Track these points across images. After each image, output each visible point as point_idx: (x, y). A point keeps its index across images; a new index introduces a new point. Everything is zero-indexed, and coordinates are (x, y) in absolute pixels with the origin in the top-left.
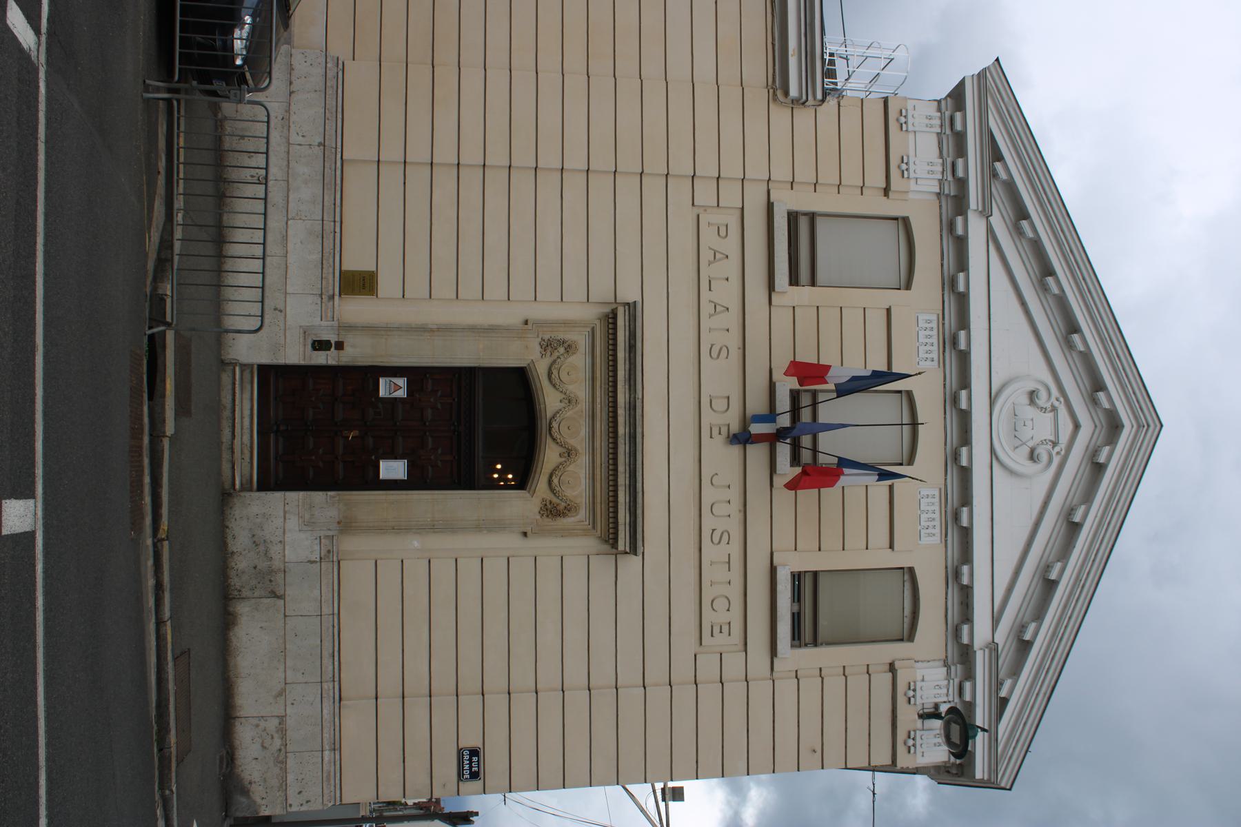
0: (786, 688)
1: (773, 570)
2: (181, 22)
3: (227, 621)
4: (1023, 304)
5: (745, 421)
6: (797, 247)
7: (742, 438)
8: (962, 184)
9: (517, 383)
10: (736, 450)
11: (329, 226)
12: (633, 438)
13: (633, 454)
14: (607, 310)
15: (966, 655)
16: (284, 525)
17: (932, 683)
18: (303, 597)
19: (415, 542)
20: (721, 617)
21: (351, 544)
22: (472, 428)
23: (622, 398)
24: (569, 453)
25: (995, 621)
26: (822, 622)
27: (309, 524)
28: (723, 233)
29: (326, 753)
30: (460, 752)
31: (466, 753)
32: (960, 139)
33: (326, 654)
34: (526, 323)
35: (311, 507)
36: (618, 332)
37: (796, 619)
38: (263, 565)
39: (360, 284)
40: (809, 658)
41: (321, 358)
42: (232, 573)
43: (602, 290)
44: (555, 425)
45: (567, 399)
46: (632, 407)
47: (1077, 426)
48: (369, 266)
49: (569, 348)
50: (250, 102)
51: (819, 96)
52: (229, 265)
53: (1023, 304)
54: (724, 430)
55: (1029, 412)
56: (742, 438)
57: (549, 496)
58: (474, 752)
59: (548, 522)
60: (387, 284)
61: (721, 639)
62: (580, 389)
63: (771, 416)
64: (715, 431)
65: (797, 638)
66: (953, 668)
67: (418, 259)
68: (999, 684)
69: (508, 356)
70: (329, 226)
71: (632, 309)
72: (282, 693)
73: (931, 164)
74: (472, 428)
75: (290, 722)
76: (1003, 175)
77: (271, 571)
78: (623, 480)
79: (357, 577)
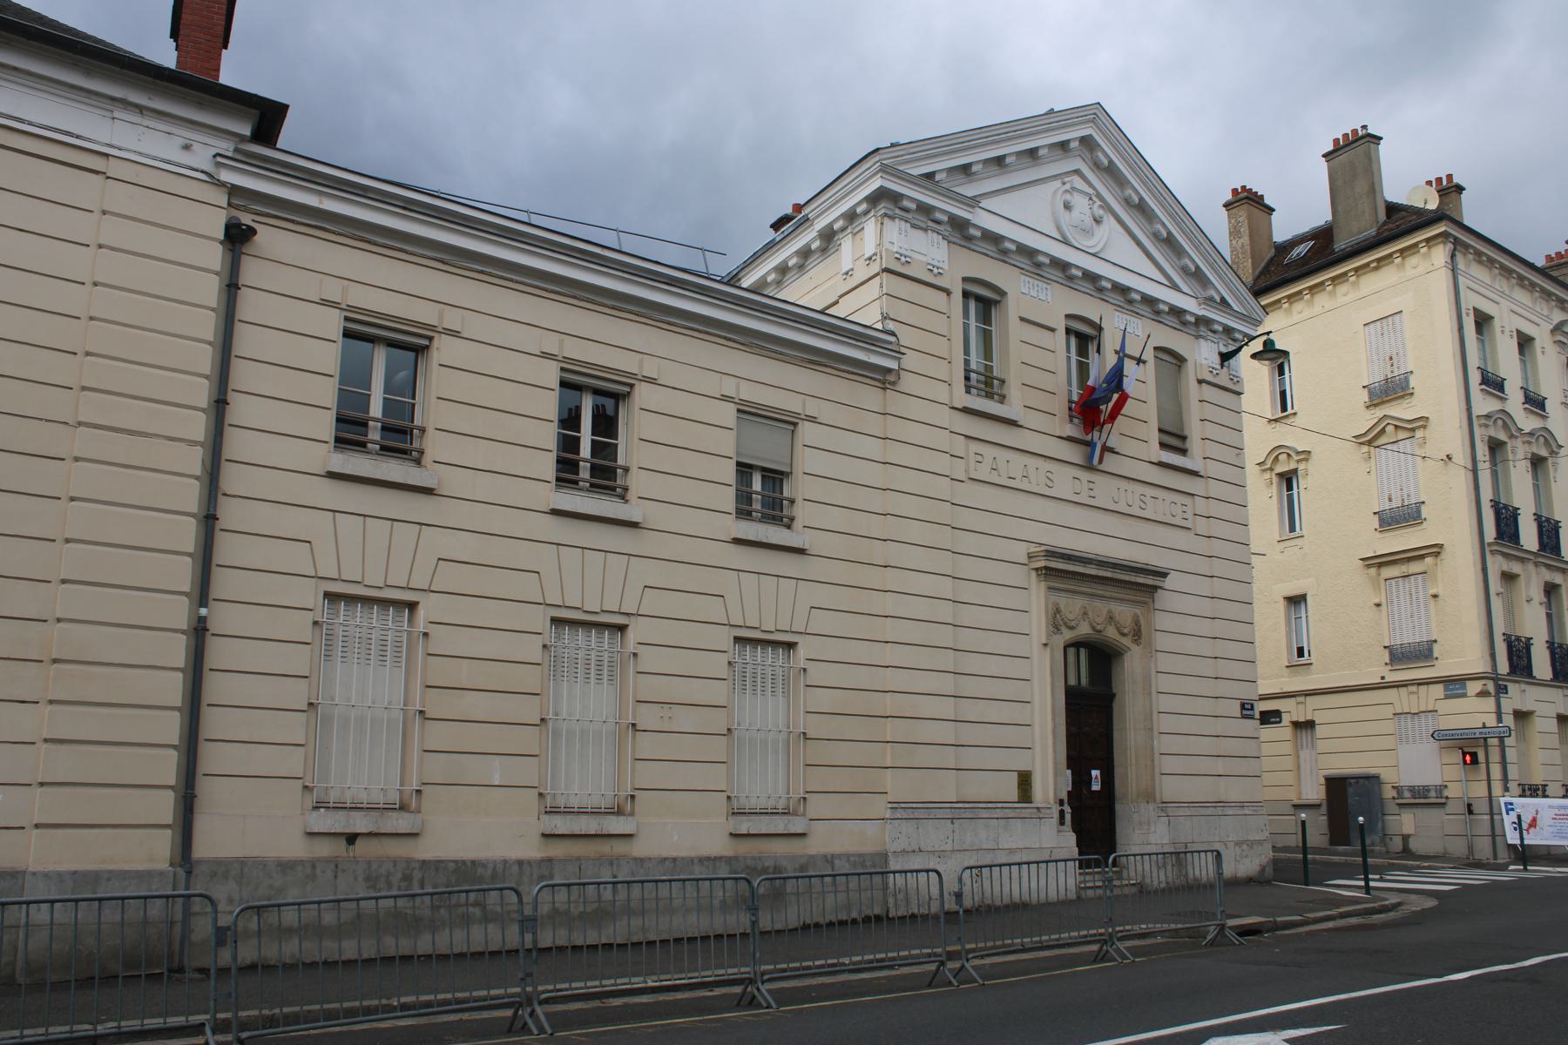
11: (999, 813)
14: (1034, 574)
15: (1201, 321)
16: (1144, 835)
18: (1194, 832)
20: (1178, 510)
24: (1111, 618)
25: (1175, 287)
39: (1025, 780)
41: (1068, 817)
43: (1018, 576)
47: (1077, 172)
50: (535, 908)
51: (892, 339)
52: (998, 903)
55: (1075, 213)
58: (1243, 706)
70: (999, 813)
71: (1051, 554)
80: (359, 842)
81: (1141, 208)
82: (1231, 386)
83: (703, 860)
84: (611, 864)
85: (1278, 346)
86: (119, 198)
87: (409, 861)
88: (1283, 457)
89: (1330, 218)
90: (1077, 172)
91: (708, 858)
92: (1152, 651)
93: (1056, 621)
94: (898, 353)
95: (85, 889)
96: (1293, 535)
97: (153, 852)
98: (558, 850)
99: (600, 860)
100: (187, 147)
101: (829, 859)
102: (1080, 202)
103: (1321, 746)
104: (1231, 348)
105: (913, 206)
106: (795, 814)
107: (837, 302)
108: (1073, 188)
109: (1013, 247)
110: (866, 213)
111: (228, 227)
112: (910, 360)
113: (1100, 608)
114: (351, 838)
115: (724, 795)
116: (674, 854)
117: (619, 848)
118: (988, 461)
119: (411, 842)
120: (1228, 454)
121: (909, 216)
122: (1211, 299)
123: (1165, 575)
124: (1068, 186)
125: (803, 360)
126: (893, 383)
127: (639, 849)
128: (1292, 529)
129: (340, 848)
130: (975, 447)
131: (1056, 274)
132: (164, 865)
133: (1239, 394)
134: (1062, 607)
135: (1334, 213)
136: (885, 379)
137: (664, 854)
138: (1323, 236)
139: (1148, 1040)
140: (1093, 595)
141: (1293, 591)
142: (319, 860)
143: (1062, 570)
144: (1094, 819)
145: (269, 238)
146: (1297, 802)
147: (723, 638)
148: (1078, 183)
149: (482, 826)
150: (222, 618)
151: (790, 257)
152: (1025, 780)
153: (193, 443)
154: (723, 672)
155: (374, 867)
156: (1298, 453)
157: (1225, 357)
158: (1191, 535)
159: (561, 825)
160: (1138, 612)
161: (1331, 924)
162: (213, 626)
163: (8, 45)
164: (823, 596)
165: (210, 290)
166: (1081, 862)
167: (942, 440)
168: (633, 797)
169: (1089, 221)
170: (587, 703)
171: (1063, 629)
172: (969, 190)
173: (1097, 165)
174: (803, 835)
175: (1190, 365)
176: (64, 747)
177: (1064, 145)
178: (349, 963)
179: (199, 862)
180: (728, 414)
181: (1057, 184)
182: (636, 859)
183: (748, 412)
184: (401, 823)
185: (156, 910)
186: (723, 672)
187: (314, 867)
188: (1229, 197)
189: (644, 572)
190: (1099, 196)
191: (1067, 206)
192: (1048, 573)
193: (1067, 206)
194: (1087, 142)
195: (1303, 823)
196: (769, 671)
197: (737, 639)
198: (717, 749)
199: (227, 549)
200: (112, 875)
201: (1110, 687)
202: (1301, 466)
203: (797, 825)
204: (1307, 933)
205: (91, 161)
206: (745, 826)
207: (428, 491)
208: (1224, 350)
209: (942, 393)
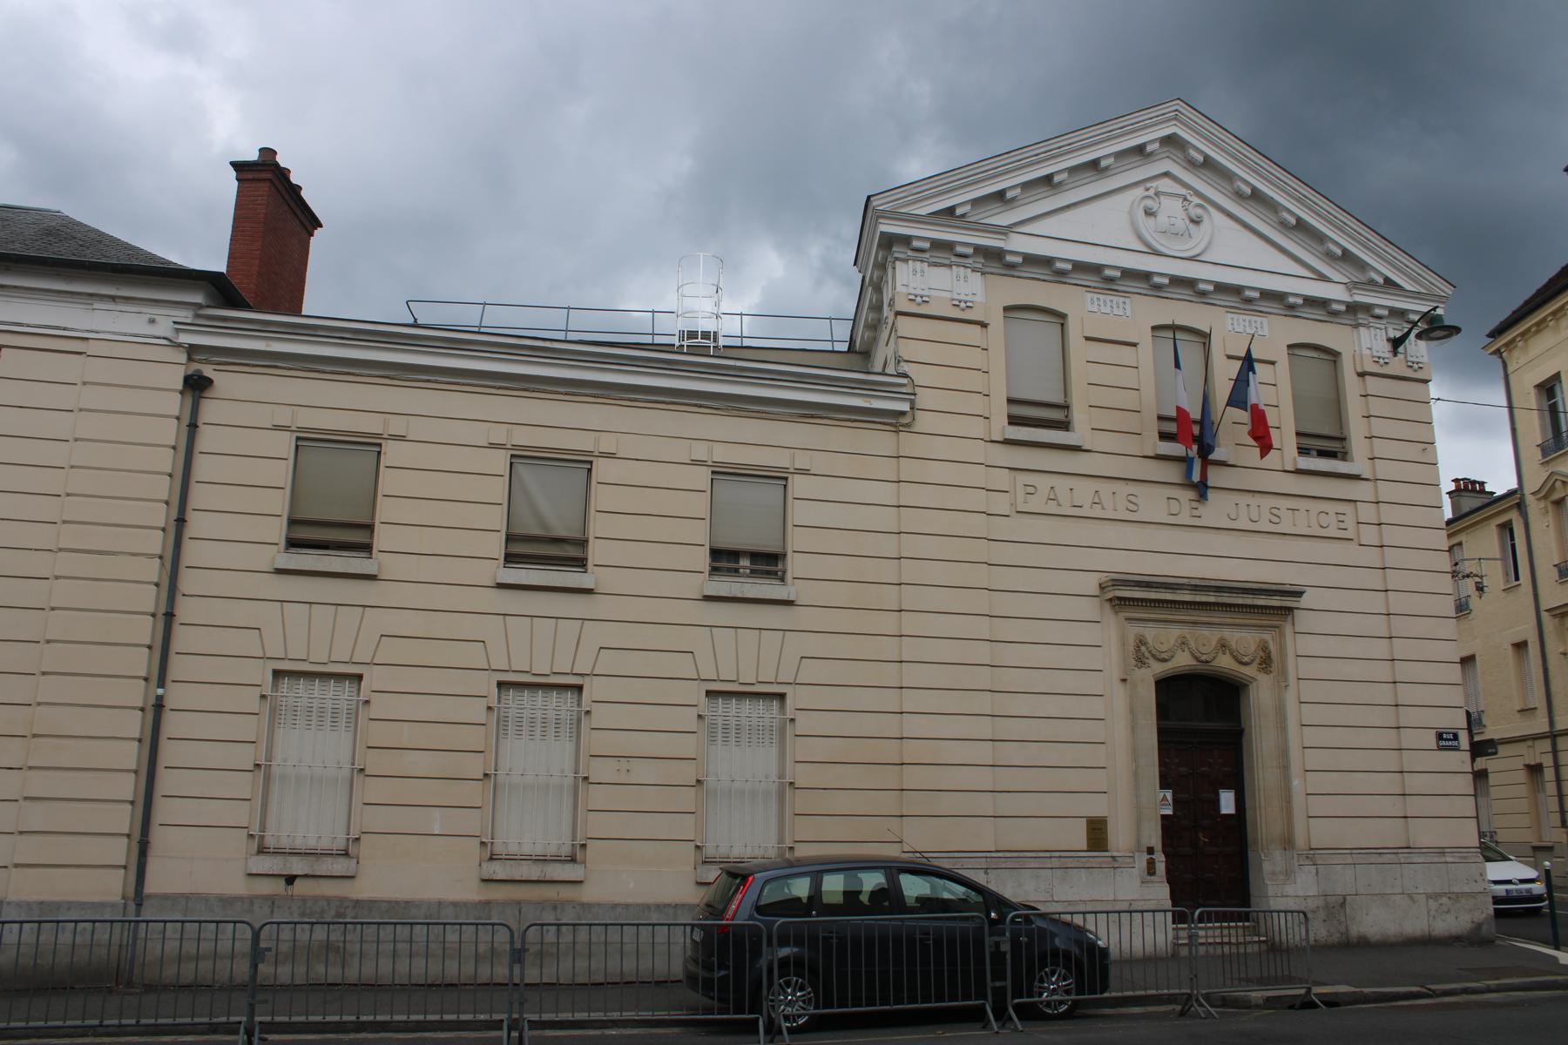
0: (1383, 469)
3: (1364, 944)
4: (1068, 207)
5: (1188, 484)
6: (1039, 418)
7: (1201, 489)
8: (979, 250)
9: (1170, 688)
10: (1211, 494)
11: (1056, 863)
12: (1219, 589)
13: (1231, 590)
14: (1107, 605)
15: (1353, 308)
16: (1286, 889)
17: (1368, 343)
18: (1344, 880)
19: (1296, 783)
20: (1331, 520)
21: (1300, 841)
22: (1202, 726)
23: (1186, 597)
24: (1223, 646)
25: (1323, 278)
26: (1326, 431)
27: (1289, 874)
28: (1031, 490)
29: (1449, 859)
30: (1440, 748)
32: (937, 245)
33: (1380, 860)
34: (1124, 680)
35: (1274, 873)
36: (1131, 597)
37: (1323, 454)
38: (1322, 914)
39: (1097, 832)
40: (1357, 445)
41: (1161, 867)
42: (1330, 940)
43: (1089, 609)
44: (1204, 658)
45: (1184, 646)
47: (1166, 174)
48: (1082, 826)
49: (1141, 642)
51: (904, 381)
53: (1068, 207)
54: (1195, 504)
55: (1162, 218)
56: (1201, 489)
57: (1255, 665)
58: (1440, 736)
59: (1275, 666)
60: (1096, 808)
61: (1350, 523)
62: (1175, 632)
63: (1185, 461)
64: (1196, 513)
65: (1343, 455)
67: (1073, 780)
68: (1372, 282)
69: (1148, 696)
70: (1056, 863)
72: (1410, 896)
73: (915, 272)
74: (1202, 726)
75: (1429, 890)
76: (967, 208)
77: (1326, 907)
78: (1249, 600)
79: (1321, 834)
80: (297, 882)
82: (1409, 373)
83: (660, 907)
84: (555, 908)
86: (97, 370)
87: (342, 900)
90: (1166, 174)
92: (1282, 683)
93: (1141, 654)
95: (46, 916)
97: (110, 888)
98: (499, 893)
99: (541, 905)
100: (152, 321)
101: (372, 904)
111: (187, 379)
114: (290, 880)
116: (630, 901)
117: (566, 893)
119: (347, 882)
120: (1412, 452)
121: (970, 261)
123: (1299, 594)
124: (1151, 192)
125: (791, 415)
127: (589, 894)
129: (279, 887)
132: (117, 898)
133: (1426, 381)
136: (896, 422)
137: (618, 900)
140: (1195, 623)
142: (257, 897)
144: (1209, 856)
145: (224, 381)
147: (695, 693)
148: (1165, 185)
149: (420, 868)
150: (175, 696)
153: (151, 556)
154: (481, 716)
155: (309, 904)
157: (1396, 343)
158: (1353, 546)
159: (499, 870)
162: (170, 703)
163: (8, 270)
164: (814, 645)
165: (169, 432)
166: (1174, 913)
167: (977, 476)
170: (536, 758)
171: (1152, 661)
172: (1003, 219)
173: (1192, 164)
176: (38, 803)
178: (285, 988)
179: (149, 896)
181: (1139, 192)
182: (582, 905)
184: (339, 866)
185: (102, 934)
186: (481, 716)
187: (252, 903)
192: (1120, 603)
196: (733, 722)
197: (708, 693)
199: (182, 639)
200: (70, 905)
205: (72, 344)
207: (789, 603)
209: (977, 428)
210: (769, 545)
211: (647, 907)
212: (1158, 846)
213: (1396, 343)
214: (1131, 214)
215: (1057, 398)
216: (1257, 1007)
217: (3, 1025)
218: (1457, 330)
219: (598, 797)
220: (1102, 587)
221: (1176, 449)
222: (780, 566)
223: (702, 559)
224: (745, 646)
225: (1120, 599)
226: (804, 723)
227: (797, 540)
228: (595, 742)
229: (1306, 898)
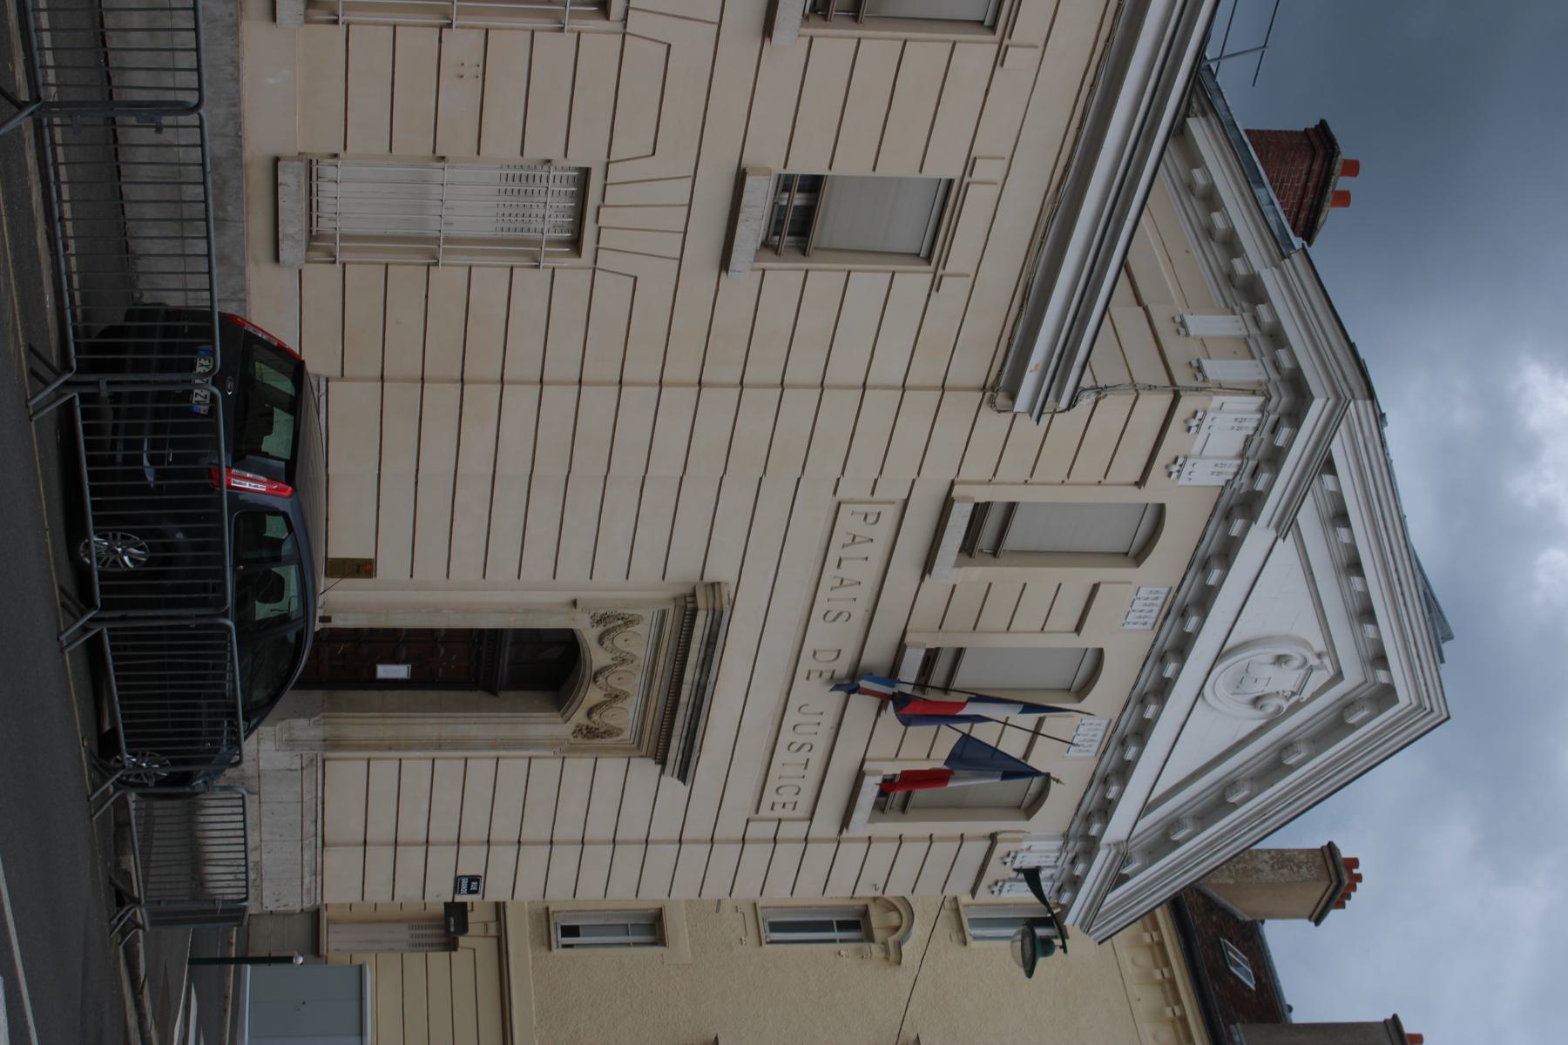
1: (948, 503)
2: (86, 442)
7: (849, 684)
10: (839, 695)
15: (1090, 847)
20: (788, 795)
23: (690, 675)
24: (615, 697)
25: (1147, 808)
27: (291, 743)
29: (306, 881)
31: (465, 882)
34: (574, 603)
39: (363, 568)
43: (684, 569)
45: (623, 673)
46: (701, 689)
47: (1338, 676)
54: (827, 675)
55: (1270, 671)
57: (586, 722)
58: (474, 879)
60: (390, 566)
66: (1071, 844)
81: (1275, 767)
85: (1041, 962)
88: (894, 919)
89: (1297, 1017)
90: (1338, 676)
91: (239, 127)
92: (565, 751)
93: (611, 622)
94: (1038, 411)
96: (764, 927)
102: (1287, 679)
103: (415, 959)
104: (1046, 887)
105: (1280, 441)
106: (309, 248)
107: (1139, 302)
108: (1311, 669)
109: (1212, 581)
110: (1276, 364)
112: (1027, 429)
113: (632, 682)
115: (339, 149)
116: (246, 79)
118: (864, 531)
121: (1265, 434)
122: (1126, 860)
123: (683, 774)
124: (1313, 661)
125: (1033, 274)
126: (992, 403)
128: (776, 927)
130: (890, 515)
131: (1168, 637)
134: (635, 628)
135: (1298, 1026)
136: (1000, 389)
138: (1266, 1003)
139: (6, 933)
140: (653, 672)
141: (676, 925)
143: (693, 626)
146: (324, 916)
147: (588, 153)
148: (1318, 679)
151: (1227, 218)
152: (363, 568)
154: (533, 153)
156: (899, 945)
157: (1032, 876)
160: (626, 735)
161: (132, 1021)
168: (336, 22)
169: (1257, 690)
171: (601, 629)
172: (1308, 517)
173: (1348, 705)
174: (277, 259)
175: (1021, 825)
177: (1380, 660)
180: (946, 166)
181: (1319, 644)
182: (236, 25)
183: (948, 197)
186: (533, 153)
188: (1346, 852)
189: (692, 44)
190: (1297, 706)
191: (1280, 660)
192: (687, 607)
193: (1280, 660)
194: (1386, 695)
195: (289, 960)
197: (585, 173)
198: (412, 140)
201: (509, 687)
202: (875, 948)
203: (291, 251)
204: (122, 996)
206: (291, 179)
207: (725, 264)
208: (1043, 874)
210: (826, 229)
211: (235, 102)
212: (328, 625)
213: (1032, 876)
214: (1287, 639)
215: (1012, 540)
216: (118, 863)
217: (43, 4)
218: (1030, 974)
219: (407, 277)
220: (714, 586)
221: (910, 669)
222: (787, 239)
223: (805, 164)
224: (655, 213)
225: (695, 611)
226: (531, 283)
227: (824, 279)
228: (490, 281)
229: (257, 760)
